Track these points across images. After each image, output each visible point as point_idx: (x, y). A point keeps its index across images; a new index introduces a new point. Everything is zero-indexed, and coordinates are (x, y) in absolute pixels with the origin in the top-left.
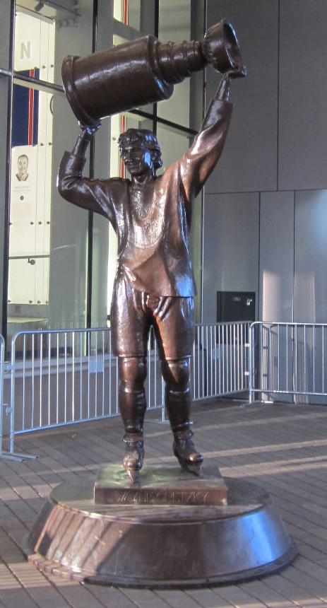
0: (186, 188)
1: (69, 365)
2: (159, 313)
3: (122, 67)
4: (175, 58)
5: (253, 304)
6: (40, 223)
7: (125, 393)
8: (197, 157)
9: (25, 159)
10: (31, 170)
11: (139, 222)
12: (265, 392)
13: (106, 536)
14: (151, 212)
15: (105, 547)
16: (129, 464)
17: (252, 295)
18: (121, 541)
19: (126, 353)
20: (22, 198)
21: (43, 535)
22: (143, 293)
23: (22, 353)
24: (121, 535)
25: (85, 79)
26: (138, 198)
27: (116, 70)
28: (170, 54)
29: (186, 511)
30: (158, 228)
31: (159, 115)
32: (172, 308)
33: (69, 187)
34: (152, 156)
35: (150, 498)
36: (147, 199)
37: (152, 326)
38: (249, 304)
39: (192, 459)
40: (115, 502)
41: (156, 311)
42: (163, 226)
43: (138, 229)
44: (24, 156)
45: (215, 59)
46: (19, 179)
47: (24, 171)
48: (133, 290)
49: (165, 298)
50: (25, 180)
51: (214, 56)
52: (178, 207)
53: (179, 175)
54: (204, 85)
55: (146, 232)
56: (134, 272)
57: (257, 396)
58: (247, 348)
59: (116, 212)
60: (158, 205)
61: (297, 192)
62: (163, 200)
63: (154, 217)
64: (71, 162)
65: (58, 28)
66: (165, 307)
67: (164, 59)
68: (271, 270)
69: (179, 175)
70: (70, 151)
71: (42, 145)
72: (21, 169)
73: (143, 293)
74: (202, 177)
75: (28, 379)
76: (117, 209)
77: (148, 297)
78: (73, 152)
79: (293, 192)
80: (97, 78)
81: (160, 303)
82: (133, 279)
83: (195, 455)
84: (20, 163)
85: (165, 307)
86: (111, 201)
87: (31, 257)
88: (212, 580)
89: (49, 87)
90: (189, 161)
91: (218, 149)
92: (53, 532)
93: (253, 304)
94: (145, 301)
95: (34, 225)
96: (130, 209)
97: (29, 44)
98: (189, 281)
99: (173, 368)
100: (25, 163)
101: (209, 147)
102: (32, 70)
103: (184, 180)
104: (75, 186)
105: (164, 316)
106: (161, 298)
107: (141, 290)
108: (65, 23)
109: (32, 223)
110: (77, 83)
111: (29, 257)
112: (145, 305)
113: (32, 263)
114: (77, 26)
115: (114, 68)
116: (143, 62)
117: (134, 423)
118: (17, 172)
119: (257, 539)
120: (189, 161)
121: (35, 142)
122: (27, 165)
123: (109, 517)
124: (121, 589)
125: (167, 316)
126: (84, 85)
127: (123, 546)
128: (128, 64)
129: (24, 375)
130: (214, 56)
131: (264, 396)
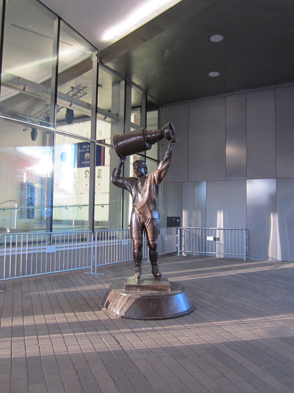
0: (156, 181)
1: (116, 242)
2: (147, 224)
3: (134, 139)
5: (179, 221)
6: (106, 193)
7: (135, 252)
9: (100, 171)
10: (102, 175)
11: (140, 193)
12: (183, 252)
13: (128, 302)
14: (144, 189)
15: (128, 305)
16: (136, 277)
17: (179, 218)
18: (134, 303)
19: (135, 238)
20: (99, 184)
21: (106, 301)
22: (141, 217)
23: (99, 238)
24: (134, 301)
25: (121, 143)
26: (139, 184)
27: (132, 140)
28: (151, 134)
29: (156, 293)
30: (146, 195)
31: (147, 155)
33: (115, 180)
35: (144, 289)
36: (143, 185)
38: (178, 221)
39: (158, 275)
40: (132, 290)
41: (146, 224)
42: (148, 194)
43: (139, 195)
44: (100, 170)
45: (166, 136)
46: (98, 178)
47: (100, 175)
48: (138, 216)
49: (149, 219)
50: (100, 178)
51: (166, 135)
52: (153, 187)
54: (163, 145)
55: (142, 196)
56: (138, 210)
57: (181, 253)
58: (177, 236)
60: (146, 187)
62: (148, 185)
63: (145, 191)
64: (116, 172)
66: (149, 222)
67: (149, 136)
68: (186, 209)
70: (116, 168)
71: (106, 166)
72: (99, 174)
73: (141, 217)
75: (101, 247)
76: (132, 188)
77: (143, 219)
78: (117, 168)
80: (125, 143)
81: (147, 221)
82: (138, 212)
84: (99, 172)
85: (149, 222)
86: (130, 185)
87: (102, 205)
89: (109, 146)
90: (157, 171)
91: (167, 167)
93: (179, 221)
94: (142, 220)
96: (137, 188)
97: (102, 130)
99: (152, 243)
100: (100, 172)
101: (164, 167)
102: (103, 140)
103: (156, 178)
104: (118, 180)
105: (148, 225)
106: (148, 219)
107: (141, 216)
108: (114, 124)
109: (103, 193)
110: (118, 144)
111: (102, 205)
112: (142, 221)
113: (103, 207)
114: (118, 125)
115: (131, 139)
116: (141, 137)
117: (138, 262)
118: (98, 175)
119: (181, 303)
120: (157, 171)
121: (104, 165)
122: (101, 173)
123: (130, 295)
125: (150, 225)
126: (121, 145)
127: (134, 305)
128: (136, 138)
129: (100, 246)
130: (166, 135)
131: (183, 253)
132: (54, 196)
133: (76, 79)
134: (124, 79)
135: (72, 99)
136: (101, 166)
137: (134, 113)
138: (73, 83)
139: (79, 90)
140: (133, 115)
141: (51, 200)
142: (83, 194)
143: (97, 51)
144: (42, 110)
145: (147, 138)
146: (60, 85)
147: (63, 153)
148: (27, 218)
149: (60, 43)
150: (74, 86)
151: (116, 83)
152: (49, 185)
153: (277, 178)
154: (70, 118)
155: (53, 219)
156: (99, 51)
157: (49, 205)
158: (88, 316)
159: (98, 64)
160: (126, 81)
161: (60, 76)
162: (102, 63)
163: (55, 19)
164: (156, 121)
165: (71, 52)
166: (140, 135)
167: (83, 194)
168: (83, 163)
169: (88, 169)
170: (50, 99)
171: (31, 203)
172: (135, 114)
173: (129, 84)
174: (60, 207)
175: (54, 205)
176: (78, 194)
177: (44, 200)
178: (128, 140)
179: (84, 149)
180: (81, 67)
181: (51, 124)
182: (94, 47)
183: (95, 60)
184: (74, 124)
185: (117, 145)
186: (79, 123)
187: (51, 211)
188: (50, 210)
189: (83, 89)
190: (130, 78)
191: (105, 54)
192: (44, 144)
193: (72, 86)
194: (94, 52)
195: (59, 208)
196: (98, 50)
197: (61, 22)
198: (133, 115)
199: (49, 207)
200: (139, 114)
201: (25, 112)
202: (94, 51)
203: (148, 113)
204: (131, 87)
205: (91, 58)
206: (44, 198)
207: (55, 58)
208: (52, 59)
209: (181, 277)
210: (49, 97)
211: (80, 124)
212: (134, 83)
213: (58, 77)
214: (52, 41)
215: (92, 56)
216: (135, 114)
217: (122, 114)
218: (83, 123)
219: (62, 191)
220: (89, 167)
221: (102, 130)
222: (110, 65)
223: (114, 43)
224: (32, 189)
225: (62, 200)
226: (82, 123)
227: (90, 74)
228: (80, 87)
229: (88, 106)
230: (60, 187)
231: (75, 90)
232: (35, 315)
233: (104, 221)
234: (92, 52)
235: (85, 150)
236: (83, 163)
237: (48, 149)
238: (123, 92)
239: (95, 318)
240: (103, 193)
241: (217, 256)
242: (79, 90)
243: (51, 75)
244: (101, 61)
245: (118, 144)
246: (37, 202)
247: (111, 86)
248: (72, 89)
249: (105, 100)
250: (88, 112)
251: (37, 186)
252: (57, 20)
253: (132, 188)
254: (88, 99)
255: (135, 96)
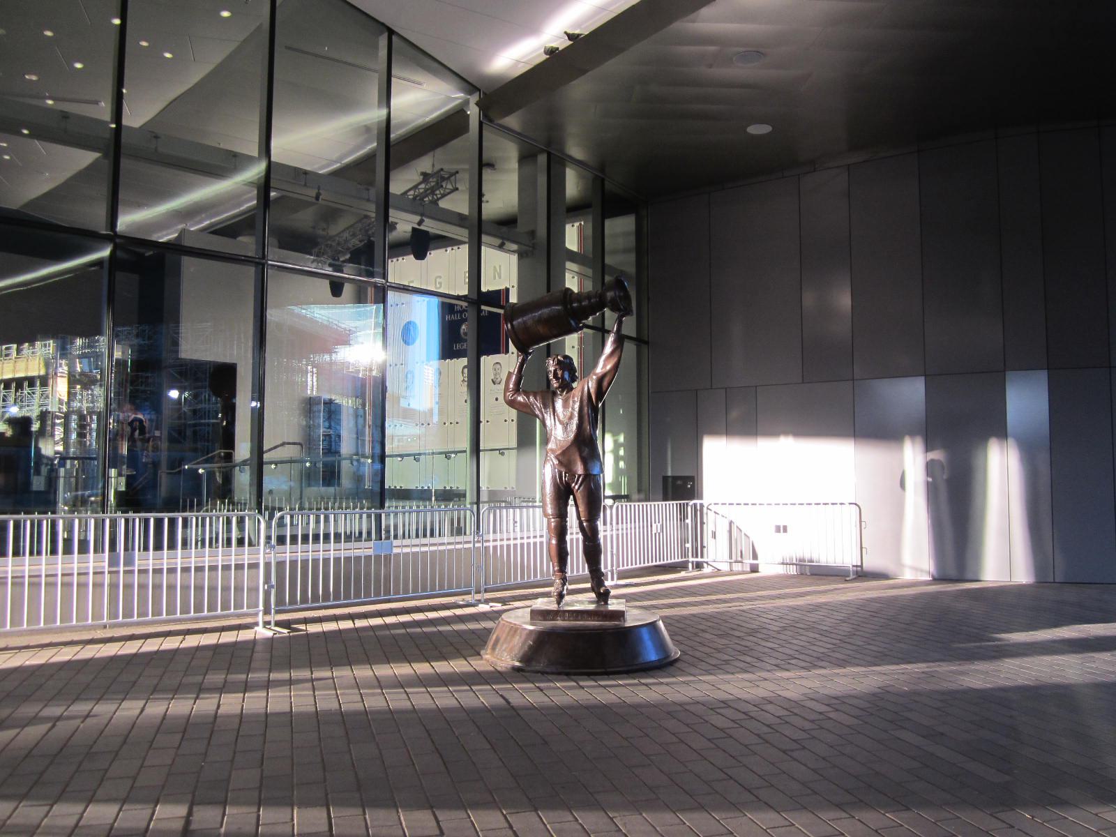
4: (583, 304)
7: (552, 544)
8: (600, 375)
9: (498, 366)
12: (62, 518)
16: (555, 594)
17: (692, 479)
19: (552, 515)
32: (585, 483)
34: (570, 374)
37: (571, 497)
44: (497, 363)
46: (494, 383)
49: (579, 476)
53: (588, 386)
54: (648, 299)
56: (557, 457)
58: (687, 524)
59: (545, 415)
61: (728, 390)
62: (577, 406)
65: (519, 259)
67: (575, 305)
69: (588, 386)
72: (495, 375)
74: (604, 389)
79: (724, 391)
82: (556, 462)
83: (604, 588)
84: (495, 370)
87: (501, 449)
88: (608, 670)
90: (594, 377)
92: (500, 636)
93: (693, 486)
94: (565, 478)
95: (507, 422)
97: (500, 266)
98: (620, 467)
101: (608, 367)
104: (516, 396)
105: (579, 489)
107: (562, 470)
109: (506, 421)
110: (514, 323)
111: (499, 450)
113: (502, 454)
115: (540, 312)
120: (594, 377)
124: (546, 675)
125: (581, 489)
128: (549, 309)
132: (388, 432)
133: (431, 154)
134: (545, 150)
135: (422, 204)
136: (500, 353)
137: (578, 221)
138: (425, 164)
139: (438, 181)
140: (575, 227)
141: (380, 440)
142: (457, 423)
143: (478, 93)
144: (355, 223)
145: (572, 307)
146: (395, 168)
147: (409, 323)
148: (323, 486)
149: (393, 79)
150: (429, 171)
151: (526, 158)
152: (376, 396)
153: (927, 373)
154: (420, 245)
155: (387, 487)
156: (483, 92)
157: (376, 455)
158: (458, 666)
159: (481, 124)
160: (549, 155)
161: (396, 148)
162: (491, 121)
163: (382, 33)
164: (632, 241)
165: (419, 99)
166: (556, 304)
167: (457, 423)
168: (456, 347)
169: (464, 361)
170: (375, 211)
171: (332, 448)
172: (580, 224)
173: (557, 163)
174: (402, 456)
175: (388, 451)
176: (445, 424)
177: (364, 441)
178: (534, 314)
179: (457, 312)
180: (444, 130)
181: (378, 270)
182: (469, 85)
183: (473, 112)
184: (432, 252)
185: (512, 325)
186: (444, 250)
187: (381, 469)
188: (378, 466)
189: (449, 178)
190: (561, 145)
191: (499, 98)
192: (360, 298)
193: (424, 171)
194: (470, 95)
195: (399, 459)
196: (480, 91)
197: (394, 38)
198: (575, 227)
199: (377, 459)
200: (590, 225)
201: (314, 228)
202: (470, 93)
203: (608, 223)
204: (564, 166)
205: (465, 109)
206: (364, 435)
207: (384, 112)
208: (376, 114)
209: (673, 609)
210: (373, 207)
211: (446, 251)
212: (570, 157)
213: (392, 150)
214: (376, 75)
215: (466, 102)
216: (580, 224)
217: (542, 231)
218: (454, 248)
219: (408, 414)
220: (466, 359)
221: (500, 266)
222: (512, 121)
223: (517, 75)
224: (332, 410)
225: (409, 440)
226: (452, 249)
227: (458, 153)
228: (442, 173)
229: (460, 220)
230: (403, 404)
231: (431, 180)
232: (354, 665)
233: (511, 489)
234: (465, 94)
235: (461, 316)
236: (456, 347)
237: (372, 308)
238: (542, 180)
239: (468, 669)
240: (507, 419)
241: (51, 341)
242: (438, 181)
243: (375, 144)
244: (485, 116)
245: (514, 323)
246: (346, 447)
247: (517, 165)
248: (423, 179)
249: (503, 194)
250: (462, 233)
251: (347, 403)
252: (386, 35)
253: (545, 413)
254: (458, 203)
255: (573, 185)
